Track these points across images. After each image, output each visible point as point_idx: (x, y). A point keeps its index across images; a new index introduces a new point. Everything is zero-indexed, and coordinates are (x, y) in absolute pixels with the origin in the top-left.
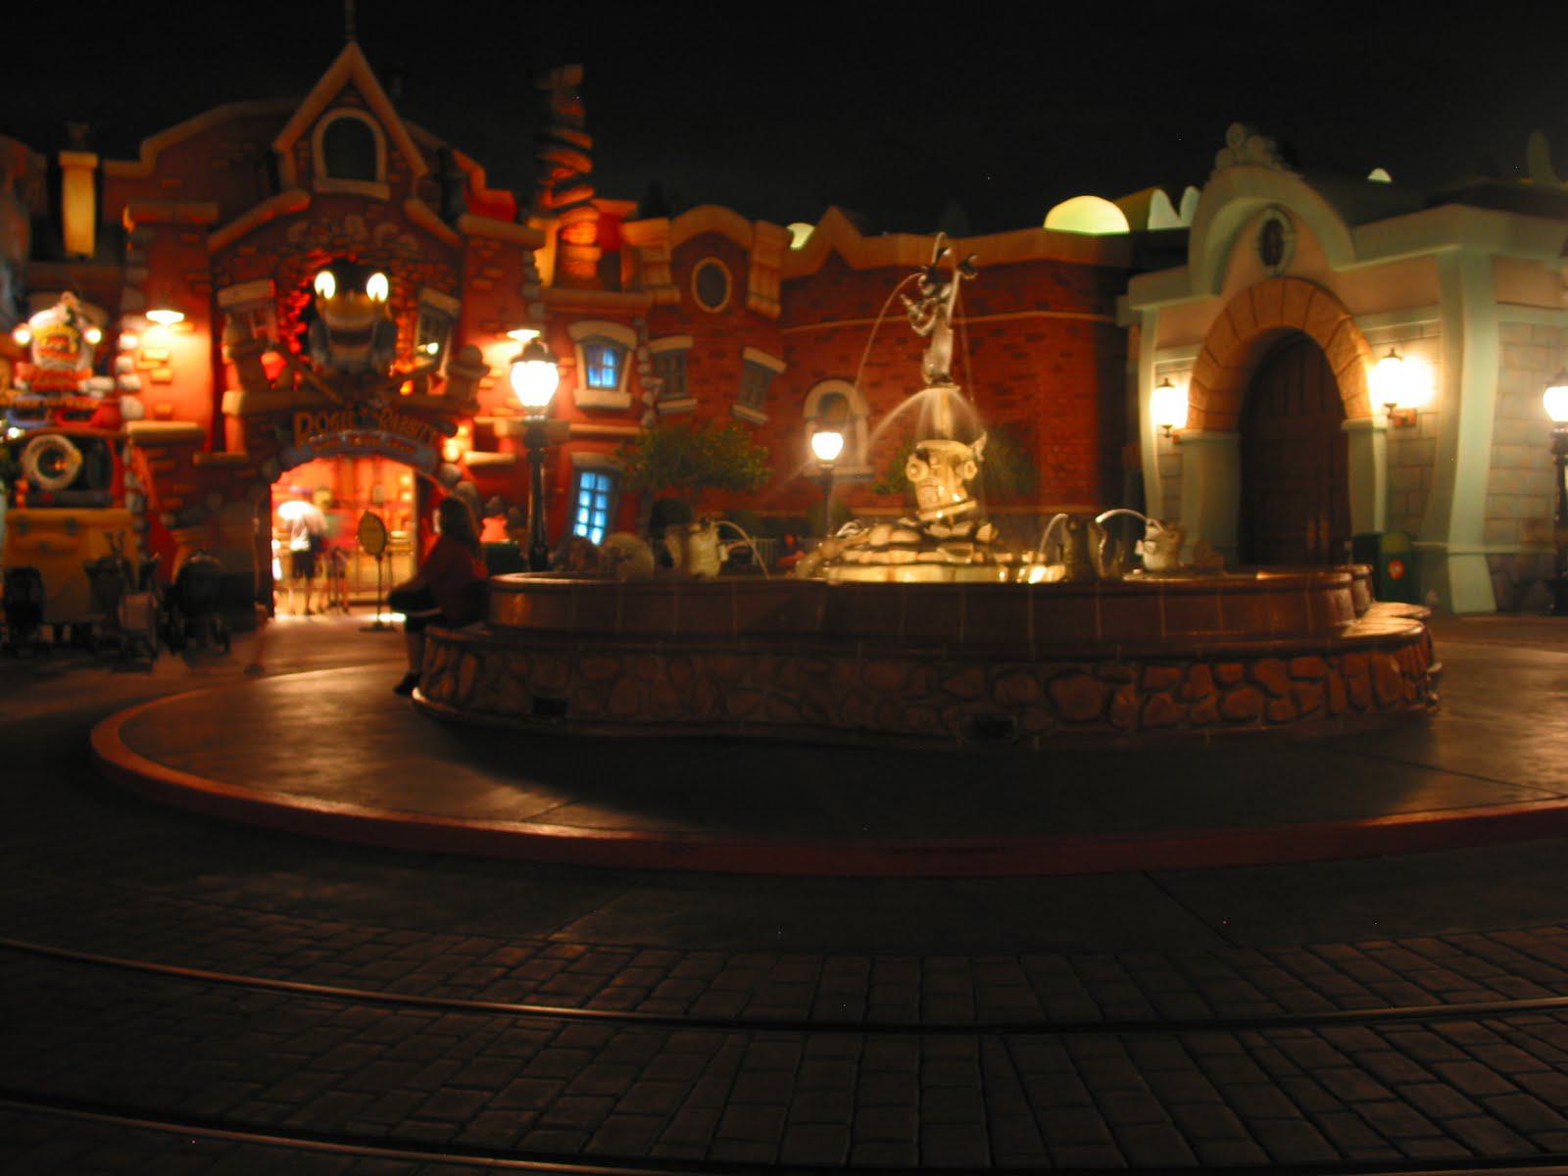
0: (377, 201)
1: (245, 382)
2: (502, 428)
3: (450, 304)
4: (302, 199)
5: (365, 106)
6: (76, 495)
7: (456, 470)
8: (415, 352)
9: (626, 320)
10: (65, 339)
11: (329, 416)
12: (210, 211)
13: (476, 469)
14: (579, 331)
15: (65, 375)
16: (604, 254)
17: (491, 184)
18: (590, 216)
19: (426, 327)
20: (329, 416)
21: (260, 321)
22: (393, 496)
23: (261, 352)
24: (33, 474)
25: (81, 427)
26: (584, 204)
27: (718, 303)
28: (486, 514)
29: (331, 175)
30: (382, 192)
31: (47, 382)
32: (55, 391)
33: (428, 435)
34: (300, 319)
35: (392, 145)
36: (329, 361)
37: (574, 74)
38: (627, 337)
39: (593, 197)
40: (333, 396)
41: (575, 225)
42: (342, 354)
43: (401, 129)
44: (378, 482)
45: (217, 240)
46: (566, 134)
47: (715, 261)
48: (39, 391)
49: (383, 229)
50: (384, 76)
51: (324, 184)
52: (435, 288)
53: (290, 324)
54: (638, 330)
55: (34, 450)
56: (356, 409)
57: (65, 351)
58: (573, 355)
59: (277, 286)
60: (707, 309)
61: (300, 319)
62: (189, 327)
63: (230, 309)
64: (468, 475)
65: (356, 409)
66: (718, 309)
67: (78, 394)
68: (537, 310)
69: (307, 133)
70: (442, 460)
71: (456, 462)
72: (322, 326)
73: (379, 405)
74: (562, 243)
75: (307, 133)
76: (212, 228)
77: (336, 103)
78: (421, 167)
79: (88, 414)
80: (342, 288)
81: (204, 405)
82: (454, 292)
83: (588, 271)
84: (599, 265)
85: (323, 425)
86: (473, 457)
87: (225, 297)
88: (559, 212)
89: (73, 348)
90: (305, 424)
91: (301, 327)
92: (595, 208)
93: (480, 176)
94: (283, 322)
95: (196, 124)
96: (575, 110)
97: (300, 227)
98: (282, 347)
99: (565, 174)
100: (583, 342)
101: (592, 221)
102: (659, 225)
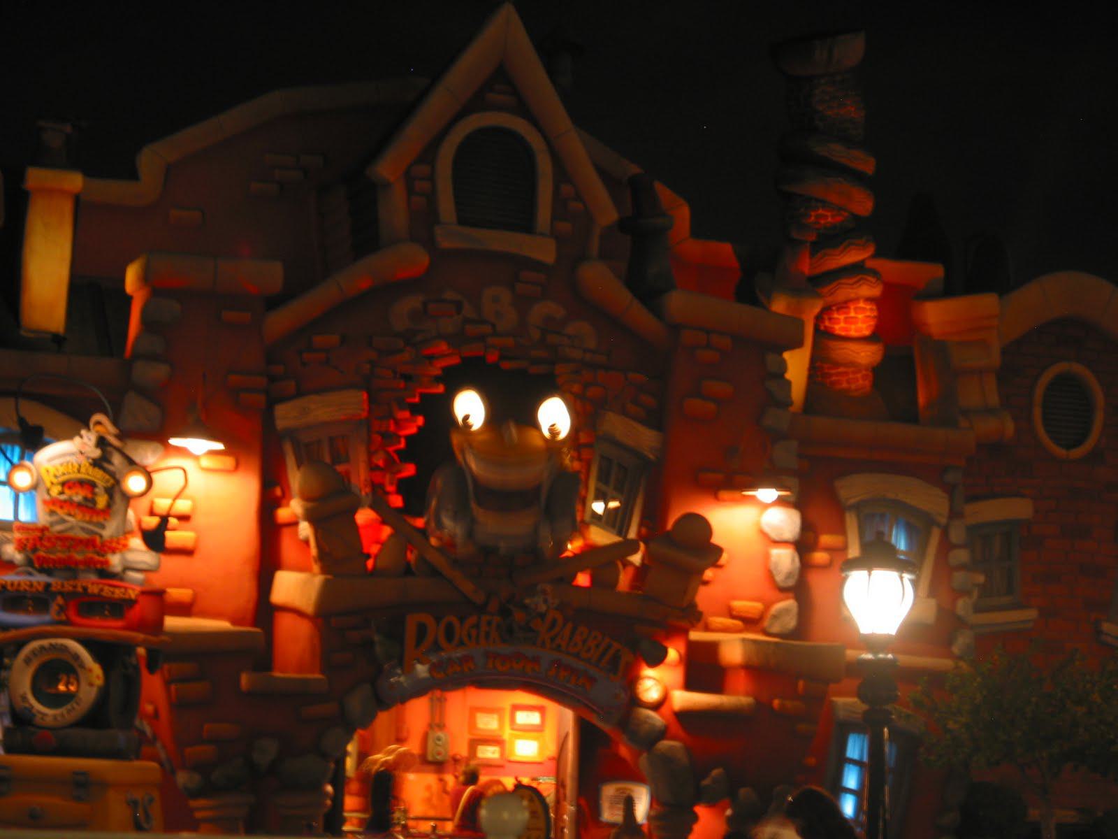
0: (538, 266)
1: (327, 561)
2: (733, 650)
3: (646, 439)
4: (415, 258)
5: (523, 109)
6: (91, 736)
7: (656, 718)
8: (587, 518)
9: (931, 473)
10: (91, 485)
11: (462, 619)
12: (271, 274)
13: (686, 717)
14: (853, 489)
15: (90, 543)
16: (887, 358)
17: (699, 230)
18: (870, 289)
19: (604, 477)
20: (462, 619)
21: (339, 456)
22: (463, 751)
23: (354, 511)
24: (24, 698)
25: (107, 628)
26: (856, 270)
27: (1078, 443)
28: (700, 796)
29: (462, 221)
30: (542, 250)
31: (60, 554)
32: (69, 568)
33: (615, 660)
34: (405, 456)
35: (562, 173)
36: (470, 534)
37: (851, 50)
38: (933, 501)
39: (874, 256)
40: (468, 587)
41: (844, 306)
42: (492, 525)
43: (576, 145)
44: (437, 724)
45: (280, 321)
46: (837, 152)
47: (1078, 368)
48: (45, 567)
49: (541, 310)
50: (548, 51)
51: (451, 235)
52: (624, 412)
53: (389, 462)
54: (949, 490)
55: (28, 661)
56: (505, 612)
57: (88, 506)
58: (841, 530)
59: (371, 400)
60: (1060, 452)
61: (405, 456)
62: (229, 462)
63: (291, 433)
64: (676, 728)
65: (505, 612)
66: (1077, 453)
67: (105, 573)
68: (785, 453)
69: (428, 154)
70: (635, 701)
71: (657, 706)
72: (461, 473)
73: (543, 608)
74: (824, 336)
75: (428, 154)
76: (273, 302)
77: (476, 103)
78: (607, 212)
79: (119, 607)
80: (493, 419)
81: (243, 592)
82: (654, 420)
83: (861, 383)
84: (878, 372)
85: (449, 633)
86: (682, 698)
87: (286, 416)
88: (818, 282)
89: (102, 502)
90: (422, 631)
91: (409, 470)
92: (874, 273)
93: (682, 214)
94: (379, 460)
95: (232, 120)
96: (851, 110)
97: (412, 302)
98: (378, 504)
99: (830, 219)
100: (857, 508)
101: (868, 300)
102: (986, 303)
